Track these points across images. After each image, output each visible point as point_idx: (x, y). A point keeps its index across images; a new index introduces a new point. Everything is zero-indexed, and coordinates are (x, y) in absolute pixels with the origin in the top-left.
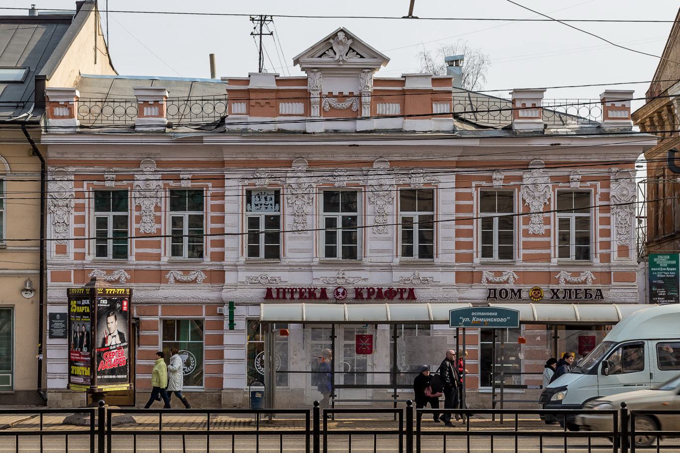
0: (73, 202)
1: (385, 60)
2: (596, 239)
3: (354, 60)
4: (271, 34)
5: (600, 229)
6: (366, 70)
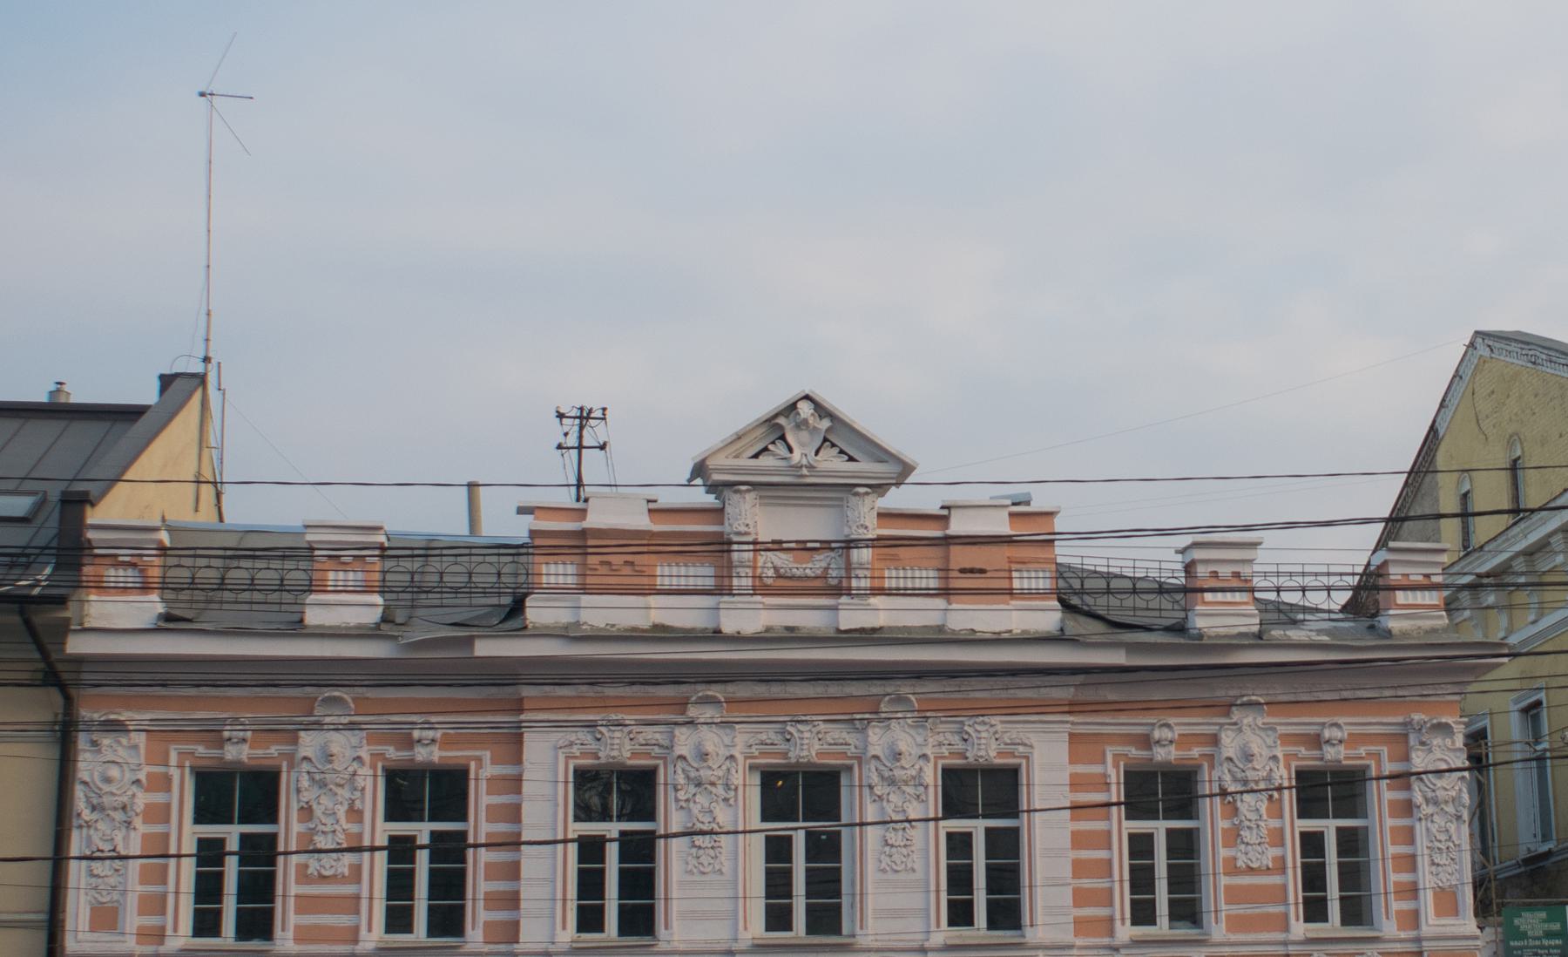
0: (142, 799)
1: (904, 471)
2: (1385, 877)
3: (831, 464)
4: (603, 447)
6: (862, 490)
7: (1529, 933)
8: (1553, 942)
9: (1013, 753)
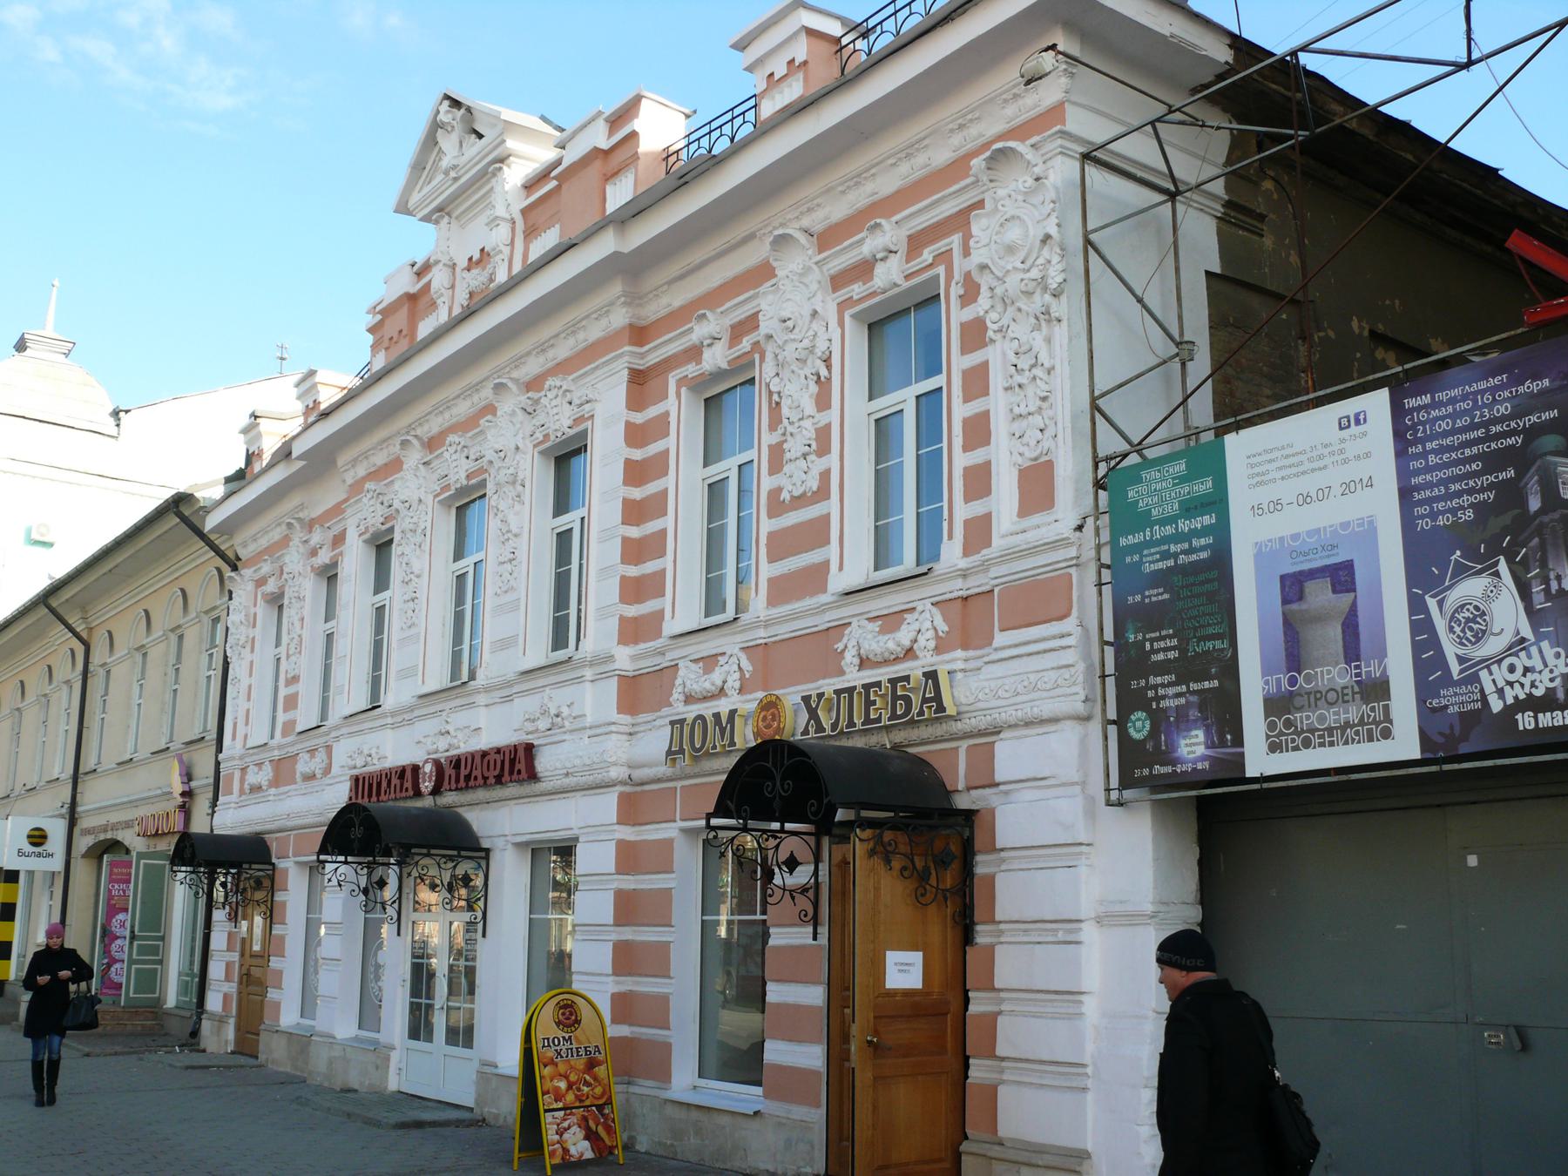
5: (232, 794)
7: (1154, 512)
8: (1197, 523)
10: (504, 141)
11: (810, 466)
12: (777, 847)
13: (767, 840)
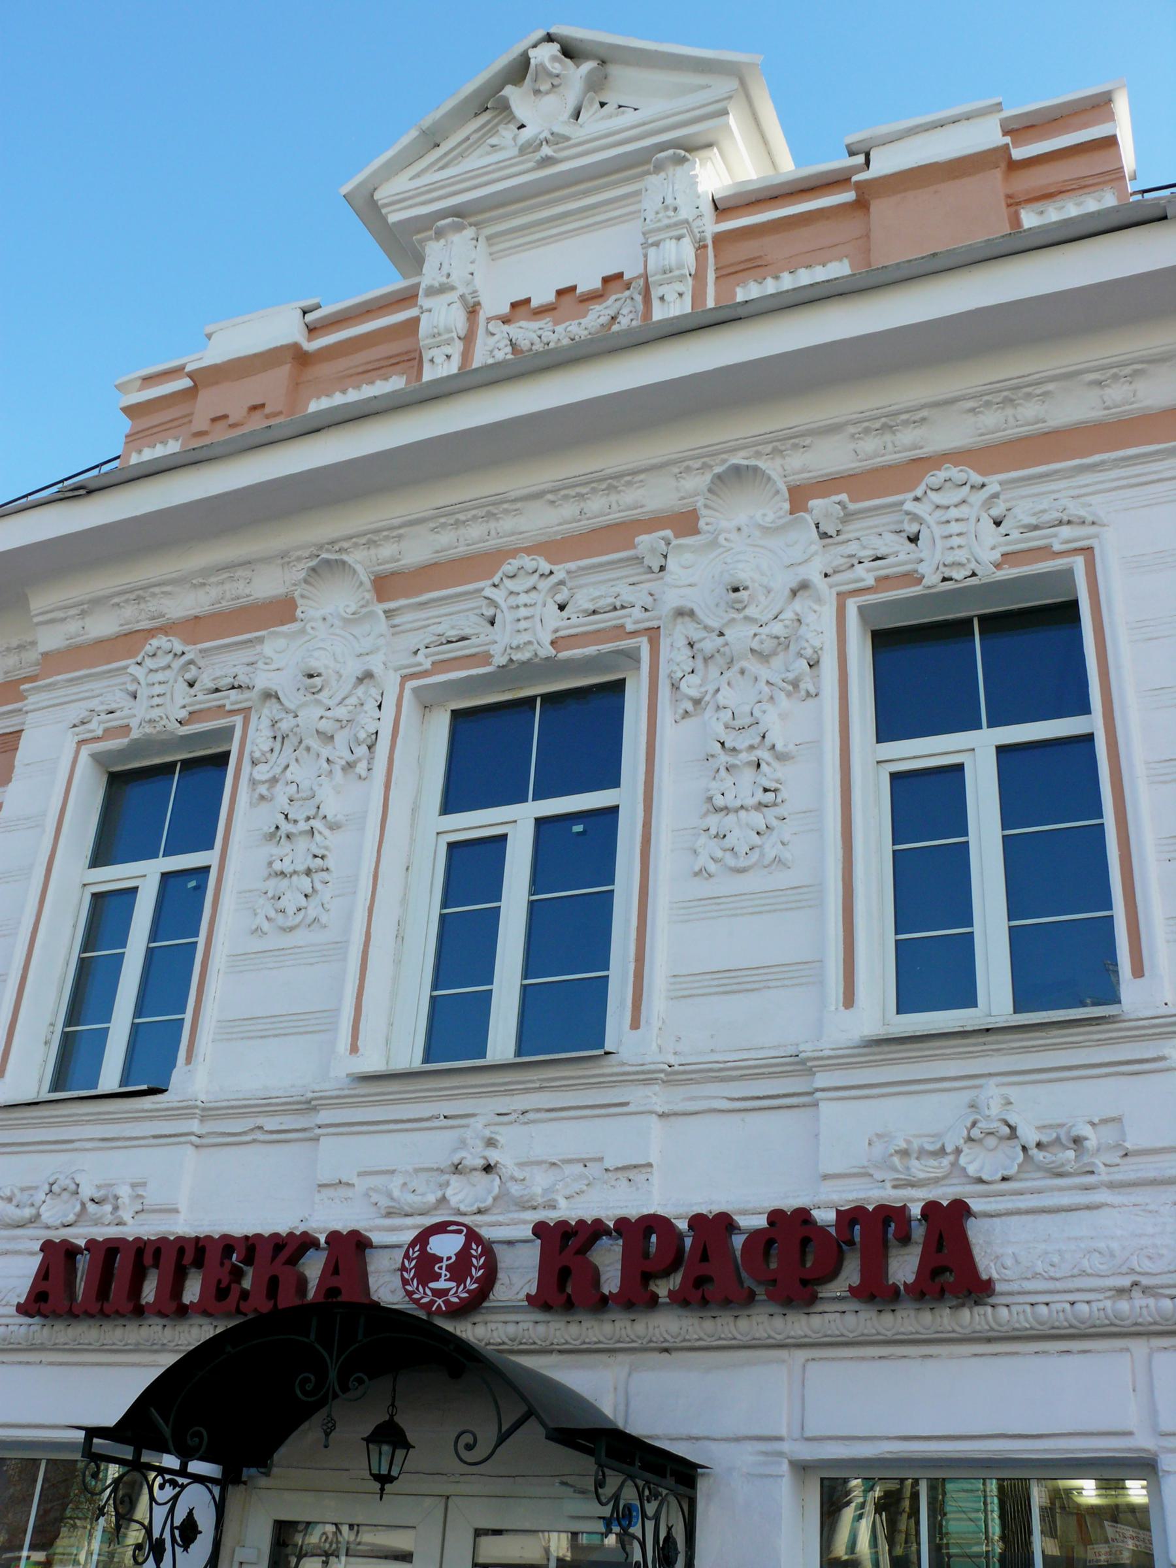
9: (622, 626)
10: (725, 113)
11: (318, 886)
12: (175, 1498)
13: (162, 1487)
